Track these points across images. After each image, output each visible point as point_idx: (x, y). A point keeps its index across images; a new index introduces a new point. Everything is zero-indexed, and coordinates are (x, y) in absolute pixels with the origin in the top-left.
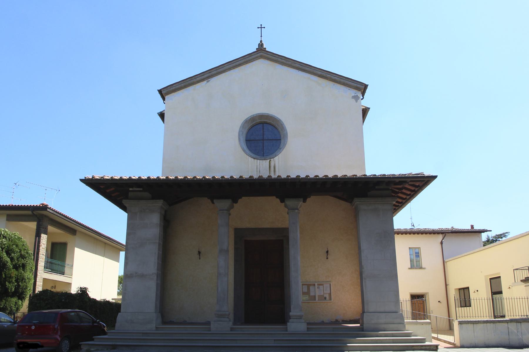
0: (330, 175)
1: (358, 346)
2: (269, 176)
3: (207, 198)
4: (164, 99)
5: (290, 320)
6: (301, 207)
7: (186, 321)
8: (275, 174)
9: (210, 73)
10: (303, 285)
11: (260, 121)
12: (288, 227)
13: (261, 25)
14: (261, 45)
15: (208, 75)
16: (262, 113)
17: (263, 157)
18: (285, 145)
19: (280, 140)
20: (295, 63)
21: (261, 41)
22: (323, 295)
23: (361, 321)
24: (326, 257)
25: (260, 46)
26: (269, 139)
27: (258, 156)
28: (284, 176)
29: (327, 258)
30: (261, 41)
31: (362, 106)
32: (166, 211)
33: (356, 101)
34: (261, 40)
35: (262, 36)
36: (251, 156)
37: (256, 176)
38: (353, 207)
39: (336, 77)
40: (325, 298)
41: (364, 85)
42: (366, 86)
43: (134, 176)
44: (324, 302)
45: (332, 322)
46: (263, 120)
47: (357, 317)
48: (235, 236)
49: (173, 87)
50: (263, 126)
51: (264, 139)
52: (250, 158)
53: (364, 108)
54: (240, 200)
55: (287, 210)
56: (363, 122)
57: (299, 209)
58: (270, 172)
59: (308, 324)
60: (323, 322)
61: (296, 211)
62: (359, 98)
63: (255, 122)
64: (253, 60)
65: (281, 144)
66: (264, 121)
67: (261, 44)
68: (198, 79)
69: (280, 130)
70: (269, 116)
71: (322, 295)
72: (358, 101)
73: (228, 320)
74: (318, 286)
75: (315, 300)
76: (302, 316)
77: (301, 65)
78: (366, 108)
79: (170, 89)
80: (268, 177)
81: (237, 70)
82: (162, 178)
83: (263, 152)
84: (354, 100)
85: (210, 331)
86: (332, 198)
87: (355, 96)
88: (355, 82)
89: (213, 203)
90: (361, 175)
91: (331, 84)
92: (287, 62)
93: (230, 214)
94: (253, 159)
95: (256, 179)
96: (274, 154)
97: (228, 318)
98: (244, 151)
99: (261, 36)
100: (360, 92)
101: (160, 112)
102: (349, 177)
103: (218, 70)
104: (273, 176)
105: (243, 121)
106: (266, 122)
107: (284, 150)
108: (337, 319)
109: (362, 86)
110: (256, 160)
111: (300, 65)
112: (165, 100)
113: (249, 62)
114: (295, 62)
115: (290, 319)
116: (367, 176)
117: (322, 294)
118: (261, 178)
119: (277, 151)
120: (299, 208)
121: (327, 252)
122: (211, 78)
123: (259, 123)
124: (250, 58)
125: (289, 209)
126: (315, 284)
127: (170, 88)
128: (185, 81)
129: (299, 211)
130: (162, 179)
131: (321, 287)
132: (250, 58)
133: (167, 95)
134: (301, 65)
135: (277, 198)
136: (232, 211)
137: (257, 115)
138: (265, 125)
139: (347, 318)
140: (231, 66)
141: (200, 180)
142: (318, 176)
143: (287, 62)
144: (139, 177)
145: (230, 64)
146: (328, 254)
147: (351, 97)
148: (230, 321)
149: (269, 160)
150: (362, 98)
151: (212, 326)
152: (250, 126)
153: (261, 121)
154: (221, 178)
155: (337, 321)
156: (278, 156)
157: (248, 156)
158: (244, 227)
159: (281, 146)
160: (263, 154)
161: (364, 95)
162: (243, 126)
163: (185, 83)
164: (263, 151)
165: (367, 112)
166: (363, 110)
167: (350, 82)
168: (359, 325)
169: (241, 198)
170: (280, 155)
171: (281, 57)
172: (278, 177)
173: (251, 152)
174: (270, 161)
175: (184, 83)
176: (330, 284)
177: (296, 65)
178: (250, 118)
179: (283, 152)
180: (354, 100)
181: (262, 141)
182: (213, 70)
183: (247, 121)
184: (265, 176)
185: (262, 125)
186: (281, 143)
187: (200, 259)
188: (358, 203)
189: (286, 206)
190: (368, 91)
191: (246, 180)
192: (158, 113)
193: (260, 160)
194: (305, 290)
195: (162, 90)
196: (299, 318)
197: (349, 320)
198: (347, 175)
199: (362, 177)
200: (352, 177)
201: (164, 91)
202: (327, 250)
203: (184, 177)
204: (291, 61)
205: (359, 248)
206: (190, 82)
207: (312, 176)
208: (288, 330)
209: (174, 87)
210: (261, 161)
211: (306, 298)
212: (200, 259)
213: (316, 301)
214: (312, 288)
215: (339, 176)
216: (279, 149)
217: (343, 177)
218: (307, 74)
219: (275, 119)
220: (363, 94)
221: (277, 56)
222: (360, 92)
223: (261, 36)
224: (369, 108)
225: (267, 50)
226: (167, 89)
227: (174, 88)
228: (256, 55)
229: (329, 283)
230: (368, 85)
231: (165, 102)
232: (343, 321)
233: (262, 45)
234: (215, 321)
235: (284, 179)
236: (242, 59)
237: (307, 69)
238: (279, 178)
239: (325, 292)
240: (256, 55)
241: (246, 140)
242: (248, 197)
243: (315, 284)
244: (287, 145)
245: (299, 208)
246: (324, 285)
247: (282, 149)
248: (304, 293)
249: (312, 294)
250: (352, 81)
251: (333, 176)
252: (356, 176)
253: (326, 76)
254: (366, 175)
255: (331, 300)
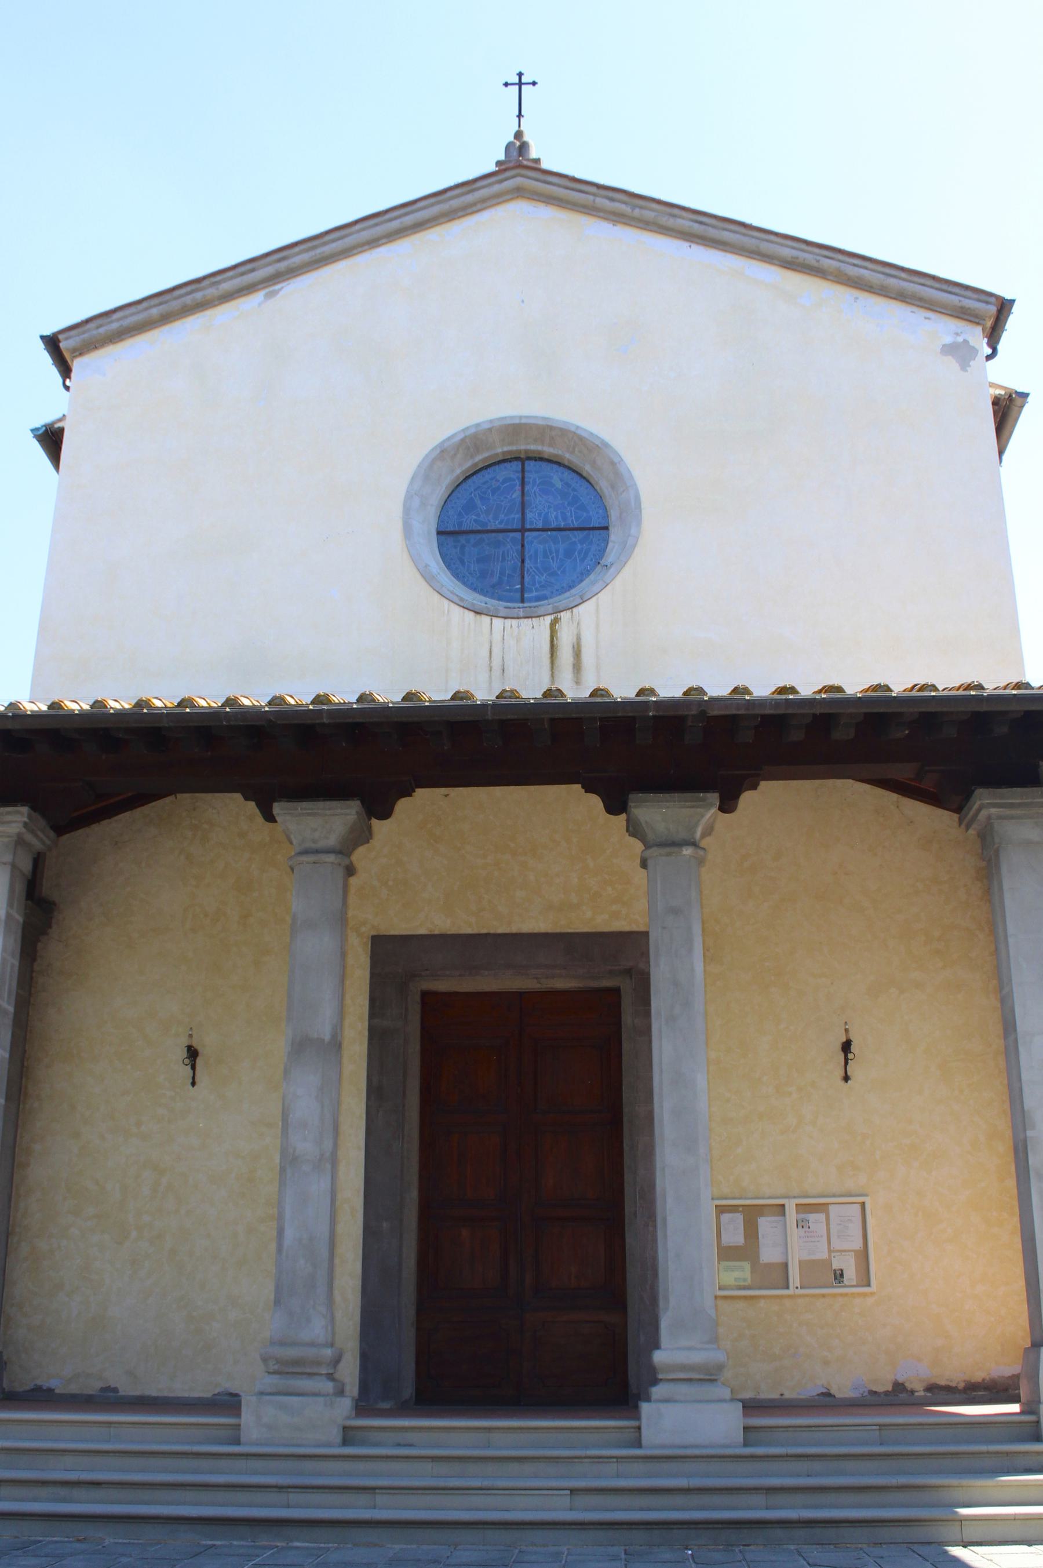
0: (854, 686)
1: (1015, 1518)
2: (550, 690)
3: (238, 796)
4: (65, 370)
5: (656, 1391)
6: (709, 831)
7: (115, 1390)
8: (578, 682)
9: (279, 260)
10: (721, 1210)
11: (506, 449)
12: (642, 929)
13: (520, 75)
14: (519, 147)
15: (270, 270)
16: (521, 417)
17: (521, 605)
18: (627, 549)
19: (606, 528)
20: (674, 216)
21: (519, 135)
22: (828, 1263)
23: (1024, 1392)
24: (842, 1073)
25: (515, 153)
26: (553, 526)
27: (495, 602)
28: (623, 691)
29: (846, 1078)
30: (519, 135)
31: (992, 385)
32: (38, 861)
33: (964, 365)
34: (517, 128)
35: (523, 113)
36: (462, 599)
37: (483, 693)
38: (971, 831)
39: (866, 268)
40: (839, 1276)
41: (993, 300)
42: (1004, 307)
43: (116, 701)
44: (834, 1296)
45: (874, 1393)
46: (523, 447)
47: (1005, 1367)
48: (372, 975)
49: (112, 322)
50: (523, 471)
51: (528, 526)
52: (456, 611)
53: (1003, 392)
54: (402, 805)
55: (638, 846)
56: (1001, 453)
57: (704, 843)
58: (556, 672)
59: (751, 1407)
60: (828, 1394)
61: (687, 851)
62: (974, 351)
63: (486, 455)
64: (479, 206)
65: (610, 545)
66: (526, 451)
67: (518, 144)
68: (226, 286)
69: (603, 485)
70: (551, 428)
71: (823, 1261)
72: (972, 363)
73: (329, 1387)
74: (802, 1216)
75: (788, 1288)
76: (720, 1367)
77: (701, 223)
78: (1010, 396)
79: (95, 332)
80: (545, 695)
81: (403, 247)
82: (29, 707)
83: (522, 584)
84: (952, 363)
85: (237, 1442)
86: (867, 787)
87: (954, 343)
88: (950, 289)
89: (270, 818)
90: (1002, 685)
91: (844, 295)
92: (637, 212)
93: (350, 871)
94: (470, 616)
95: (484, 706)
96: (573, 591)
97: (330, 1377)
98: (429, 579)
99: (520, 115)
100: (979, 329)
101: (42, 426)
102: (946, 693)
103: (319, 251)
104: (574, 691)
105: (430, 448)
106: (539, 452)
107: (627, 571)
108: (900, 1380)
109: (987, 303)
110: (486, 619)
111: (696, 222)
112: (73, 375)
113: (460, 214)
114: (676, 211)
115: (655, 1381)
116: (1032, 688)
117: (823, 1255)
118: (513, 701)
119: (592, 577)
120: (704, 835)
121: (846, 1047)
122: (284, 281)
123: (501, 458)
124: (470, 198)
125: (647, 846)
126: (783, 1206)
127: (98, 327)
128: (167, 297)
129: (701, 853)
130: (115, 709)
131: (816, 1220)
132: (470, 198)
133: (81, 354)
134: (701, 223)
135: (588, 789)
136: (360, 856)
137: (497, 424)
138: (530, 465)
139: (953, 1373)
140: (379, 230)
141: (213, 715)
142: (792, 690)
143: (637, 212)
144: (53, 706)
145: (376, 225)
146: (850, 1056)
147: (939, 350)
148: (340, 1392)
149: (548, 619)
150: (989, 351)
151: (247, 1417)
152: (458, 471)
153: (514, 448)
154: (313, 703)
155: (899, 1387)
156: (594, 599)
157: (446, 602)
158: (422, 931)
159: (610, 557)
160: (522, 591)
161: (998, 342)
162: (427, 471)
163: (166, 302)
164: (523, 577)
165: (1015, 409)
166: (996, 402)
167: (932, 287)
168: (1015, 1408)
169: (410, 795)
170: (604, 596)
171: (611, 194)
172: (593, 694)
173: (464, 583)
174: (553, 624)
175: (161, 304)
176: (863, 1204)
177: (680, 221)
178: (463, 440)
179: (618, 582)
180: (954, 361)
181: (518, 535)
182: (297, 249)
183: (443, 453)
184: (531, 691)
185: (516, 466)
186: (606, 541)
187: (193, 1084)
188: (993, 811)
189: (634, 829)
190: (1013, 324)
191: (437, 709)
192: (32, 430)
193: (505, 618)
194: (734, 1234)
195: (61, 337)
196: (702, 1377)
197: (961, 1385)
198: (934, 686)
199: (1008, 692)
200: (961, 692)
201: (66, 339)
202: (844, 1040)
203: (133, 702)
204: (654, 206)
205: (1009, 1026)
206: (188, 300)
207: (762, 689)
208: (644, 1442)
209: (118, 320)
210: (508, 622)
211: (737, 1274)
212: (193, 1084)
213: (790, 1292)
214: (766, 1225)
215: (898, 688)
216: (599, 567)
217: (914, 693)
218: (729, 256)
219: (581, 439)
220: (994, 335)
221: (593, 190)
222: (979, 329)
223: (520, 115)
224: (1025, 396)
225: (545, 165)
226: (84, 333)
227: (115, 326)
228: (496, 188)
229: (861, 1199)
230: (1012, 302)
231: (68, 382)
232: (931, 1388)
233: (523, 148)
234: (262, 1393)
235: (626, 704)
236: (432, 205)
237: (726, 236)
238: (599, 700)
239: (836, 1244)
240: (496, 188)
241: (439, 533)
242: (443, 791)
243: (783, 1206)
244: (637, 550)
245: (704, 835)
246: (831, 1207)
247: (612, 570)
248: (727, 1253)
249: (769, 1254)
250: (937, 285)
251: (867, 690)
252: (980, 687)
253: (816, 264)
254: (1028, 684)
255: (869, 1285)
